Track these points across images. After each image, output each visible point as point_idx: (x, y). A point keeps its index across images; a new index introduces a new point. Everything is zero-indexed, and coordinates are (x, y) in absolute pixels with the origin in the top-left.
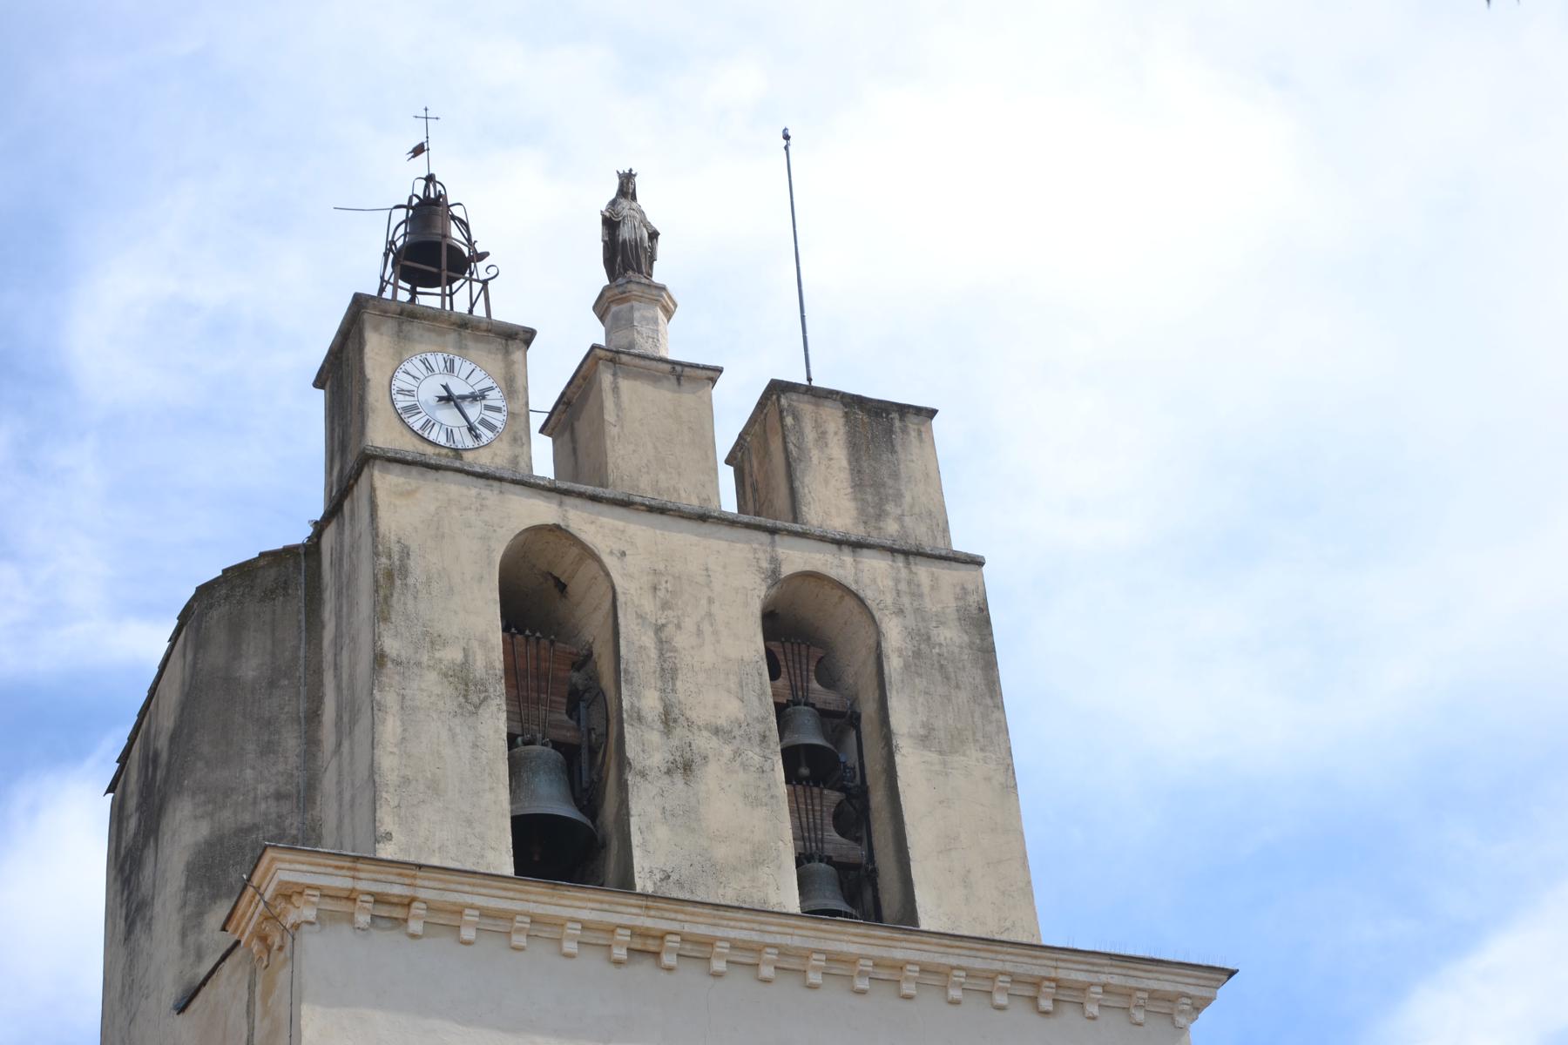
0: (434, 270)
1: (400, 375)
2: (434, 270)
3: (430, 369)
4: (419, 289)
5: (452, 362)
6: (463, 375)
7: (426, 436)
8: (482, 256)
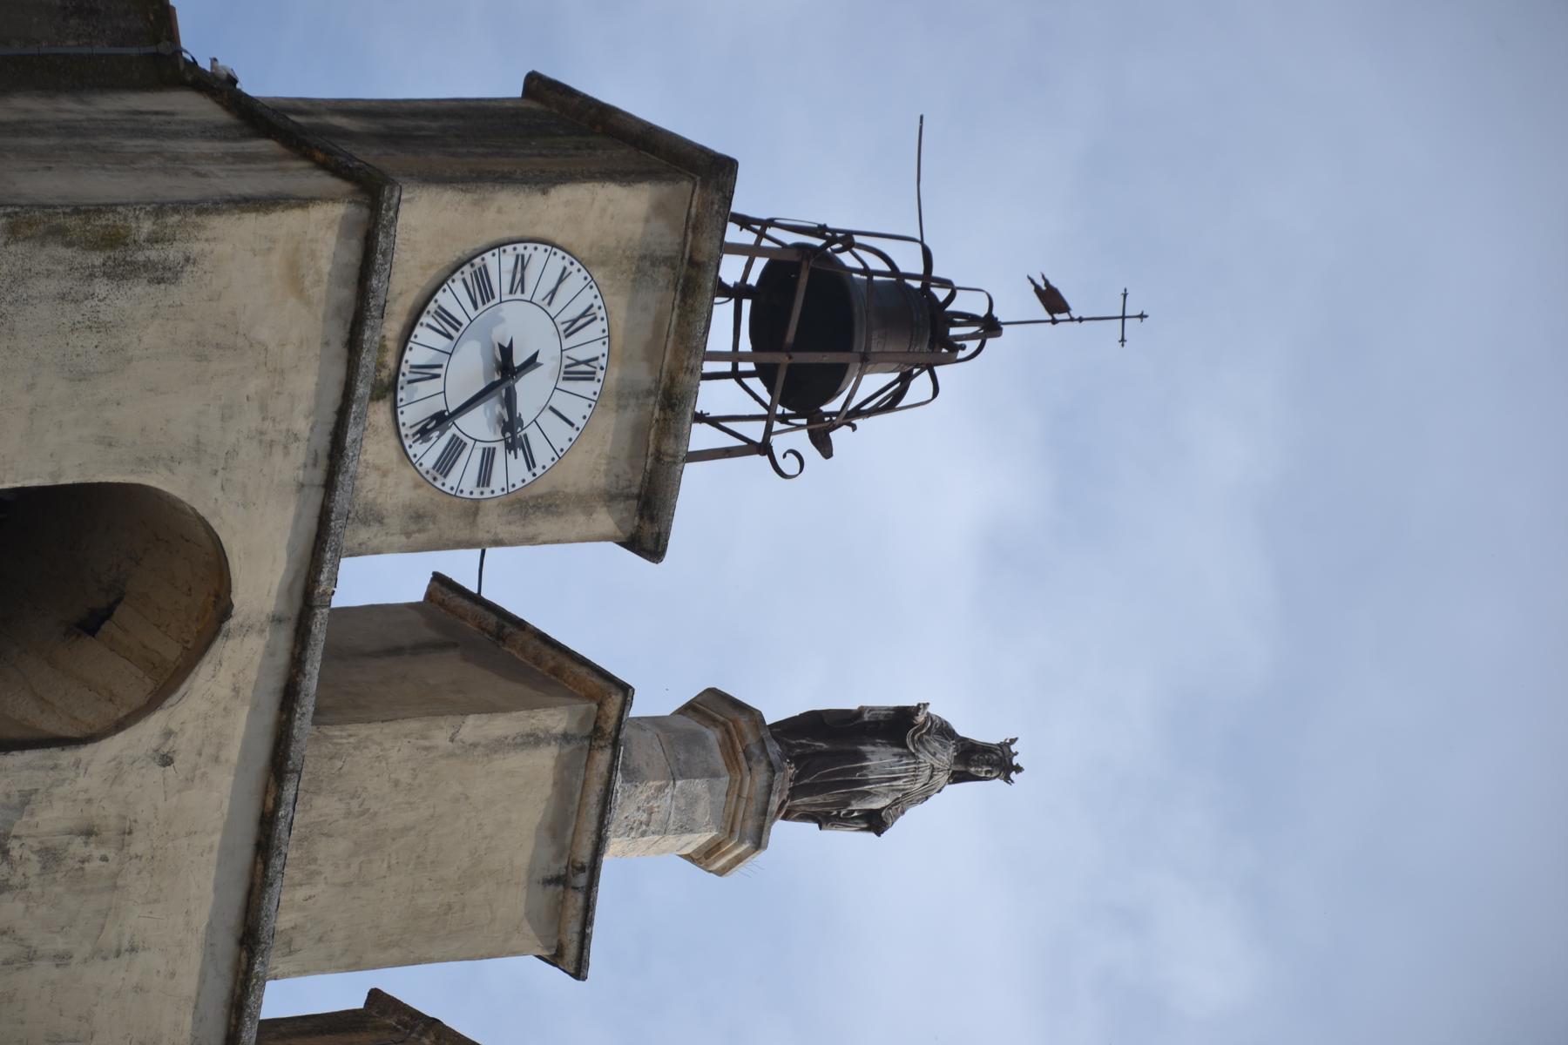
0: (790, 337)
1: (558, 262)
2: (790, 337)
3: (572, 328)
4: (747, 304)
5: (589, 377)
6: (560, 402)
7: (425, 319)
8: (824, 445)
